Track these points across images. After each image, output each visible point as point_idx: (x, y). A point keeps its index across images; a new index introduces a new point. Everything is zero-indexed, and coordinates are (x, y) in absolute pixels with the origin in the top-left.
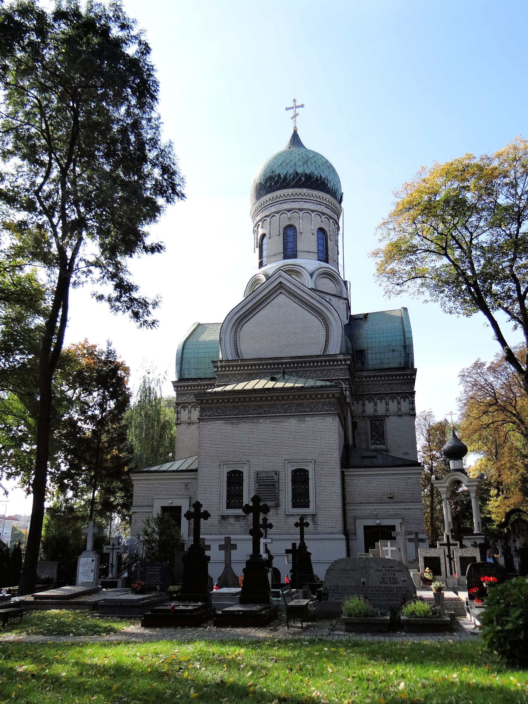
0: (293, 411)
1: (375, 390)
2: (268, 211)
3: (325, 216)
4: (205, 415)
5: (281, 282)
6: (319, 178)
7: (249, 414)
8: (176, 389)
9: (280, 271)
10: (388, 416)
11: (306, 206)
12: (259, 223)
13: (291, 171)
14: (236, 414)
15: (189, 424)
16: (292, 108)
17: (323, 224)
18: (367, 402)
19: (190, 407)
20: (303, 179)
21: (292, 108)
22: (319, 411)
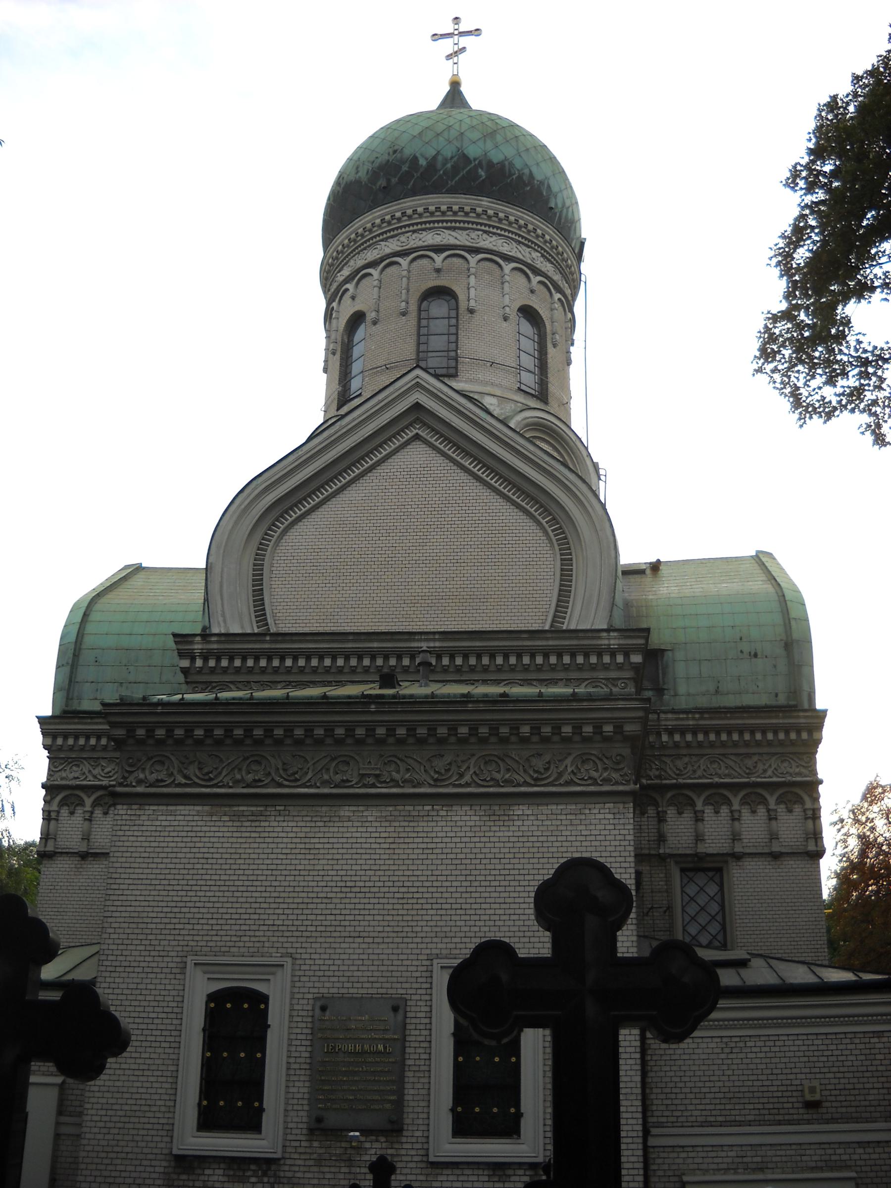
0: (467, 778)
1: (699, 773)
2: (375, 252)
3: (539, 278)
4: (140, 782)
5: (417, 406)
6: (525, 178)
7: (304, 786)
8: (49, 742)
9: (418, 372)
10: (738, 857)
11: (487, 242)
12: (347, 286)
13: (448, 152)
14: (255, 783)
15: (84, 856)
16: (449, 35)
17: (533, 297)
18: (671, 812)
19: (88, 801)
20: (482, 173)
21: (449, 35)
22: (568, 783)
